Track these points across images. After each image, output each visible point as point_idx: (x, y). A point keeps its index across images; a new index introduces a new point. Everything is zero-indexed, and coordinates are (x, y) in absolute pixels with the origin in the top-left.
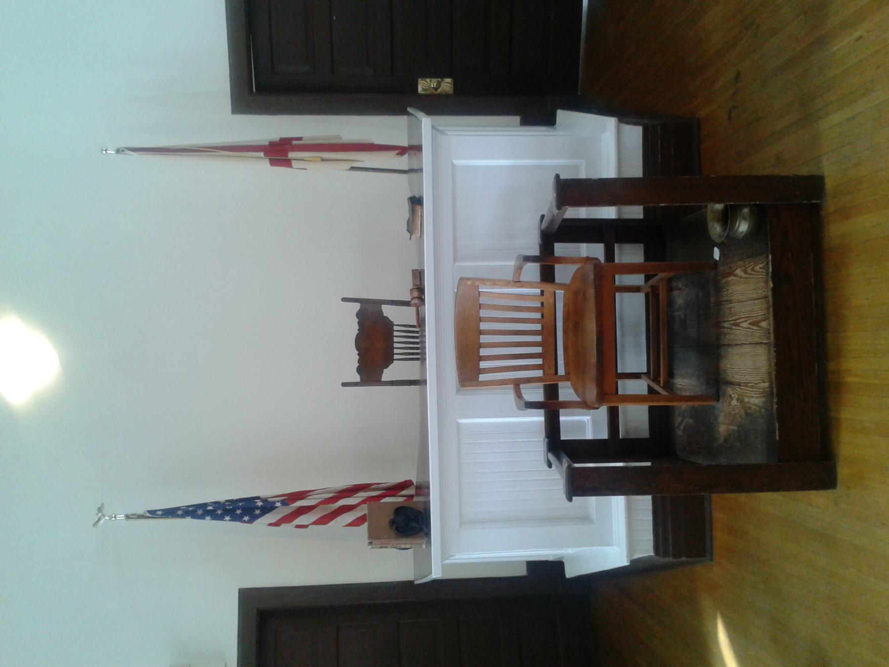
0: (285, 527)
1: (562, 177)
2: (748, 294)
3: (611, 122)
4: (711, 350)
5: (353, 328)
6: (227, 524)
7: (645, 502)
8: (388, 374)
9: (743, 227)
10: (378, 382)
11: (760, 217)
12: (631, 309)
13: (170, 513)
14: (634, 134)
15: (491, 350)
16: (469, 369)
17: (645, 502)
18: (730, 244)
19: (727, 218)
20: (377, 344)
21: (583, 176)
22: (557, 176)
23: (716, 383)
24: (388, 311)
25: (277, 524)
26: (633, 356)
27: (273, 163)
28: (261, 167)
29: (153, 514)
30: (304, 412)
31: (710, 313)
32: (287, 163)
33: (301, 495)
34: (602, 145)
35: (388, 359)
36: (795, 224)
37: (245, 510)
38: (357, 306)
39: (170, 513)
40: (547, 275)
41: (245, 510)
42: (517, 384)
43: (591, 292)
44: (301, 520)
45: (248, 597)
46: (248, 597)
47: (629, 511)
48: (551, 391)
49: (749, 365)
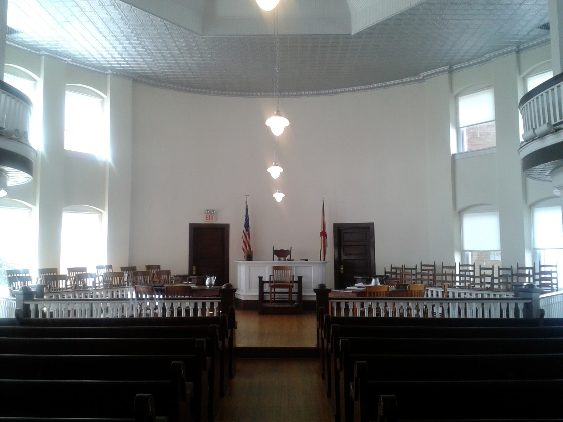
0: (243, 234)
6: (244, 222)
7: (257, 299)
8: (275, 256)
13: (247, 210)
16: (275, 268)
17: (257, 299)
20: (281, 254)
21: (303, 290)
27: (321, 233)
28: (320, 230)
29: (247, 206)
30: (269, 239)
32: (321, 236)
33: (249, 238)
35: (278, 256)
37: (247, 226)
39: (247, 210)
41: (247, 226)
42: (274, 276)
45: (228, 225)
46: (228, 225)
47: (255, 296)
48: (272, 282)
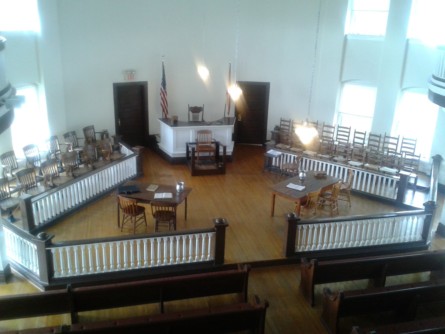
0: (160, 91)
1: (227, 228)
2: (213, 167)
3: (232, 151)
4: (204, 164)
5: (198, 106)
7: (185, 156)
8: (191, 113)
9: (220, 166)
10: (189, 110)
11: (221, 168)
12: (207, 154)
14: (230, 154)
15: (203, 135)
18: (218, 165)
19: (221, 165)
22: (227, 225)
23: (200, 164)
24: (201, 113)
25: (161, 89)
26: (201, 154)
29: (163, 67)
31: (209, 163)
34: (230, 150)
35: (193, 112)
36: (221, 172)
37: (164, 84)
38: (202, 107)
40: (212, 143)
41: (164, 84)
43: (210, 149)
44: (162, 95)
49: (204, 167)
